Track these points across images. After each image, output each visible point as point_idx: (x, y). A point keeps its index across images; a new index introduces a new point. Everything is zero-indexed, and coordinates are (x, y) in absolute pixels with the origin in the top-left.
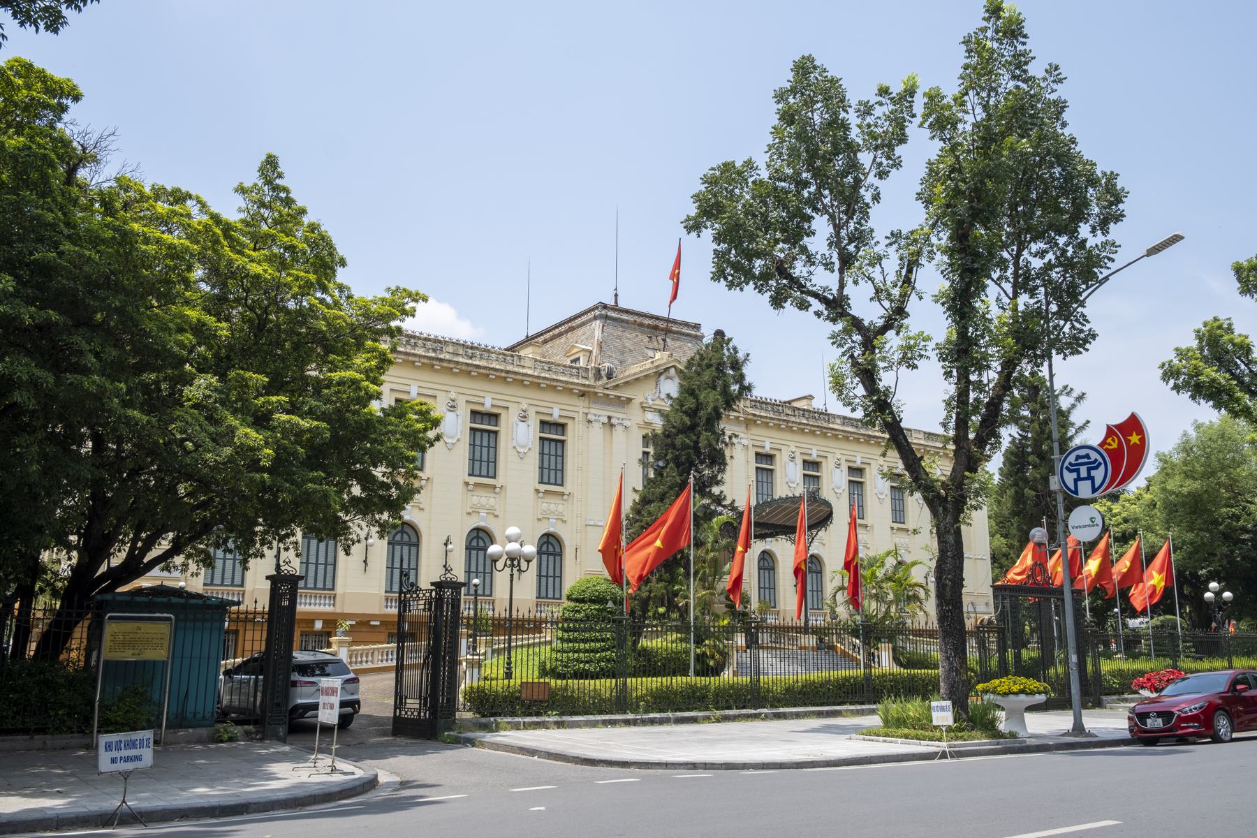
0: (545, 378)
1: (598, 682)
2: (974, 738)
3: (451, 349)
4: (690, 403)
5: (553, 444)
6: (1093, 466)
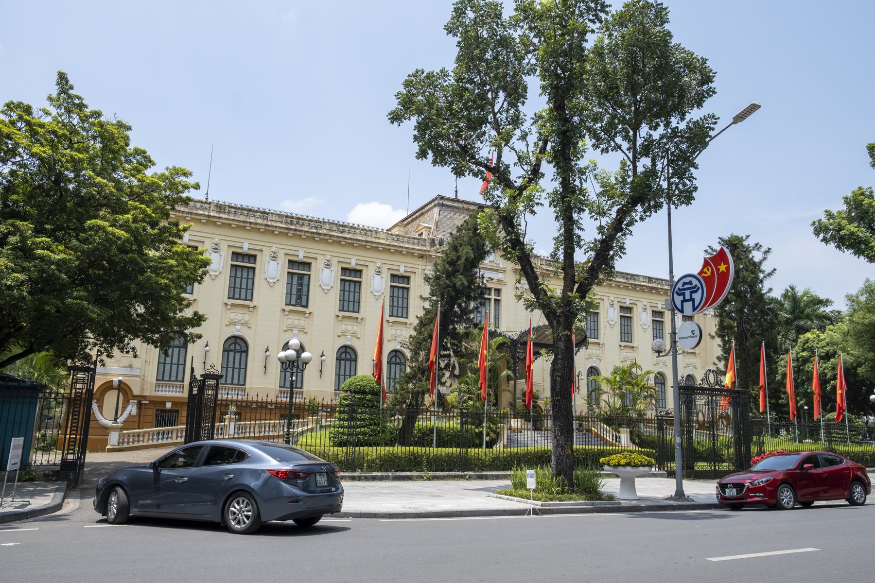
0: (393, 246)
1: (370, 448)
2: (570, 499)
3: (327, 227)
4: (453, 255)
6: (694, 290)
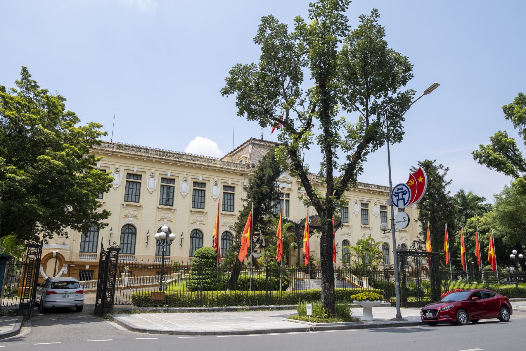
0: (225, 168)
1: (211, 292)
2: (333, 321)
3: (185, 157)
4: (261, 174)
5: (229, 195)
6: (404, 193)
